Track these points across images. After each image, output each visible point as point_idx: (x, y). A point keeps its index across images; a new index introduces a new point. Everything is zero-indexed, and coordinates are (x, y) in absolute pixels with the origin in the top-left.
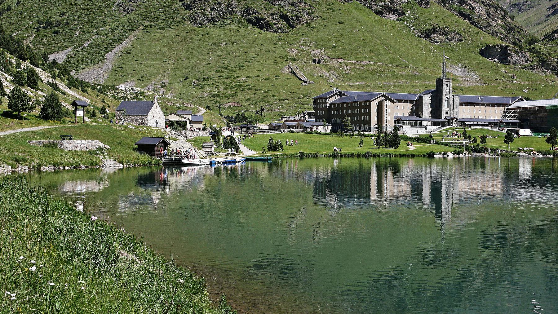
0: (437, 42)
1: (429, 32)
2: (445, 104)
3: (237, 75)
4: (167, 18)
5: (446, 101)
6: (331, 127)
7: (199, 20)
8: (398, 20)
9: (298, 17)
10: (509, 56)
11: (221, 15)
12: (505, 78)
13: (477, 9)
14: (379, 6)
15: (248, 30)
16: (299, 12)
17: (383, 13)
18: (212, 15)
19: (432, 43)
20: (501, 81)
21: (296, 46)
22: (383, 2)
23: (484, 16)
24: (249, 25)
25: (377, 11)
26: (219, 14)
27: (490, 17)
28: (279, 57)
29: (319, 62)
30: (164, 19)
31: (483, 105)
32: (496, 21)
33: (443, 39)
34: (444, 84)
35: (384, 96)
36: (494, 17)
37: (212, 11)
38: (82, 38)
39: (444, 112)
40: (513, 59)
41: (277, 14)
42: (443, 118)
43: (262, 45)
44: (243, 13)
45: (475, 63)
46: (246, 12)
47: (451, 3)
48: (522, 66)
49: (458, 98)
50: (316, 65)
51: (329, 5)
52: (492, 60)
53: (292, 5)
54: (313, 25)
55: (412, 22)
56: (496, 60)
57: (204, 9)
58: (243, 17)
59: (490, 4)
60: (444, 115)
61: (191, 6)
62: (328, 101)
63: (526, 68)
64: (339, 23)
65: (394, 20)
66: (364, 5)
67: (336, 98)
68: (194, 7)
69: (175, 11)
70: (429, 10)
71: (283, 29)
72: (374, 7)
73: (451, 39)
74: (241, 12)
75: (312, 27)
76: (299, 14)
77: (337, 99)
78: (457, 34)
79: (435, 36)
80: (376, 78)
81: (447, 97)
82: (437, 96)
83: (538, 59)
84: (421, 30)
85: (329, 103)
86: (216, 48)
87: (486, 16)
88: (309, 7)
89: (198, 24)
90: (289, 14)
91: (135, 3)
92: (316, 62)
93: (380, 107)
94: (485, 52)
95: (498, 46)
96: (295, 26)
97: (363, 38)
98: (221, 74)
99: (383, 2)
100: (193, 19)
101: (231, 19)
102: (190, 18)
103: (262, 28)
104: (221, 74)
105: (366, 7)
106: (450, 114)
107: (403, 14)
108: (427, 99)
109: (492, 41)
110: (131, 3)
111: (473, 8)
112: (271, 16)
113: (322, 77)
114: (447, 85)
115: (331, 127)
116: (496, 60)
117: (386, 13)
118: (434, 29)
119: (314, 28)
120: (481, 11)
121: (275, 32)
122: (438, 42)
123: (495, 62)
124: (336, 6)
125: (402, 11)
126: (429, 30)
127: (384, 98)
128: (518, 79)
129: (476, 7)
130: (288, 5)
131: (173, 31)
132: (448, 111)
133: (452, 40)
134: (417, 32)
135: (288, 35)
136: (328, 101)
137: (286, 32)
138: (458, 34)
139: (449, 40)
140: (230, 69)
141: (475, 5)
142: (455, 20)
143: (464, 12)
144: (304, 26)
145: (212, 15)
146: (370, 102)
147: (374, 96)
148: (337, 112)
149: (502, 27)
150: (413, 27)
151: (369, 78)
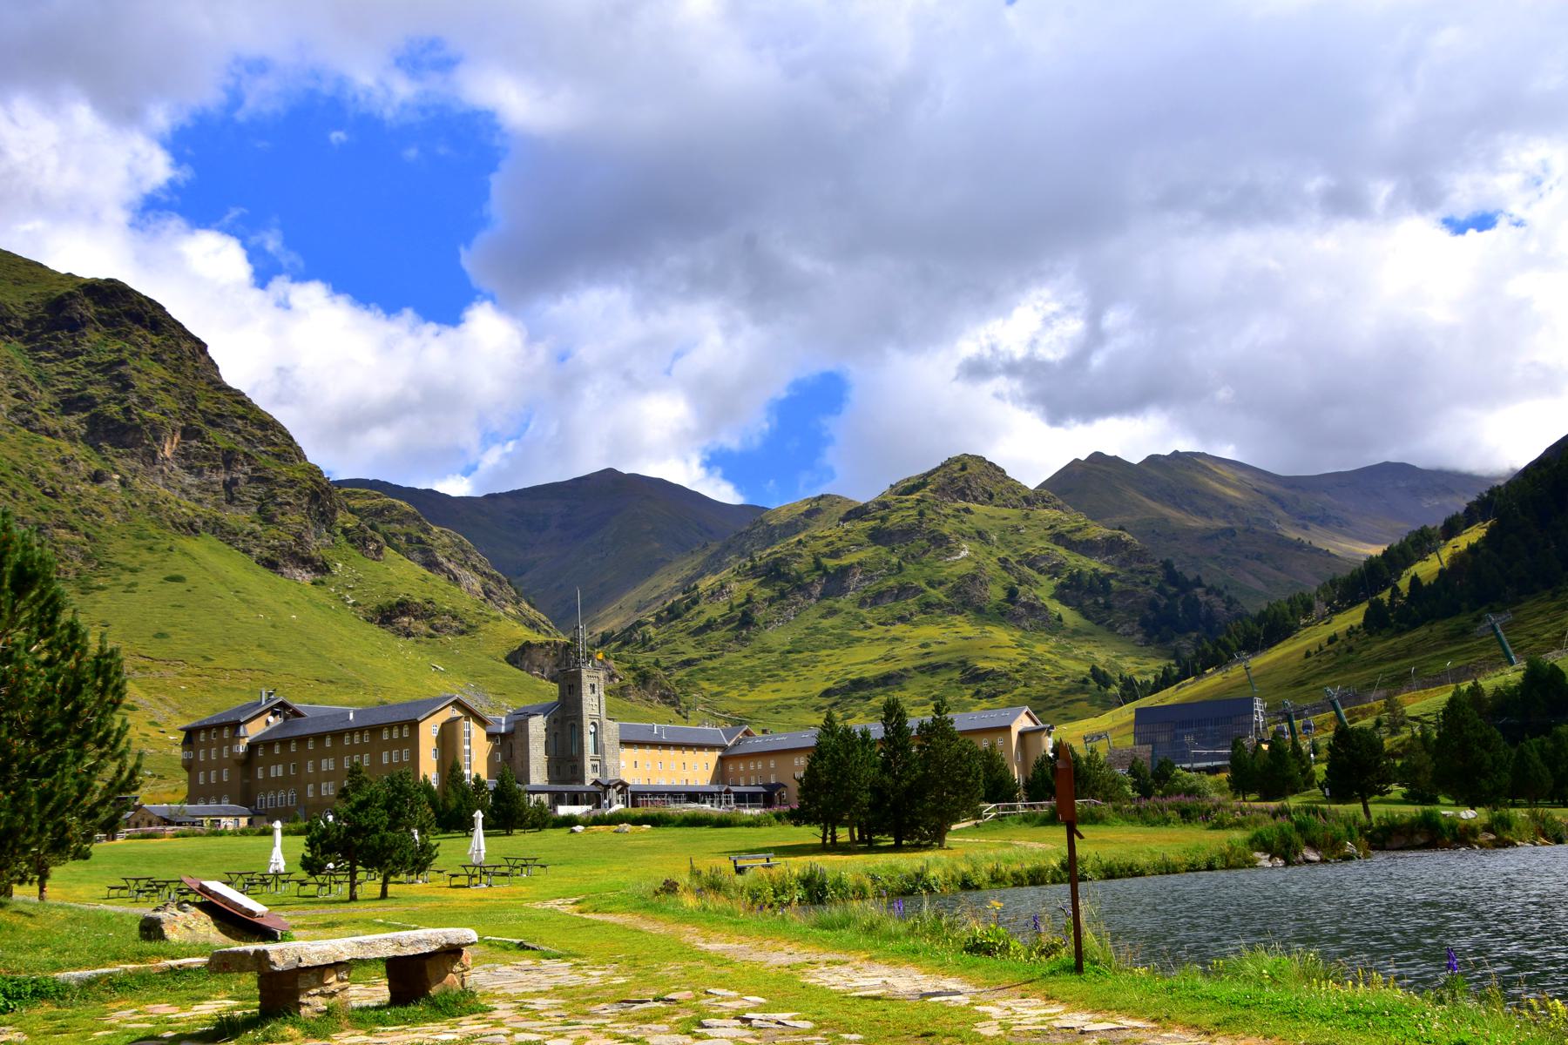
0: (408, 635)
2: (589, 740)
14: (268, 548)
27: (490, 598)
32: (502, 607)
35: (458, 704)
39: (588, 764)
42: (588, 783)
51: (139, 537)
60: (590, 776)
66: (230, 544)
67: (268, 723)
77: (271, 726)
78: (455, 618)
83: (634, 674)
84: (373, 606)
85: (247, 740)
87: (483, 595)
106: (604, 771)
107: (323, 568)
108: (537, 727)
114: (593, 686)
118: (400, 604)
125: (323, 562)
127: (458, 713)
132: (598, 763)
139: (437, 630)
146: (414, 725)
147: (431, 706)
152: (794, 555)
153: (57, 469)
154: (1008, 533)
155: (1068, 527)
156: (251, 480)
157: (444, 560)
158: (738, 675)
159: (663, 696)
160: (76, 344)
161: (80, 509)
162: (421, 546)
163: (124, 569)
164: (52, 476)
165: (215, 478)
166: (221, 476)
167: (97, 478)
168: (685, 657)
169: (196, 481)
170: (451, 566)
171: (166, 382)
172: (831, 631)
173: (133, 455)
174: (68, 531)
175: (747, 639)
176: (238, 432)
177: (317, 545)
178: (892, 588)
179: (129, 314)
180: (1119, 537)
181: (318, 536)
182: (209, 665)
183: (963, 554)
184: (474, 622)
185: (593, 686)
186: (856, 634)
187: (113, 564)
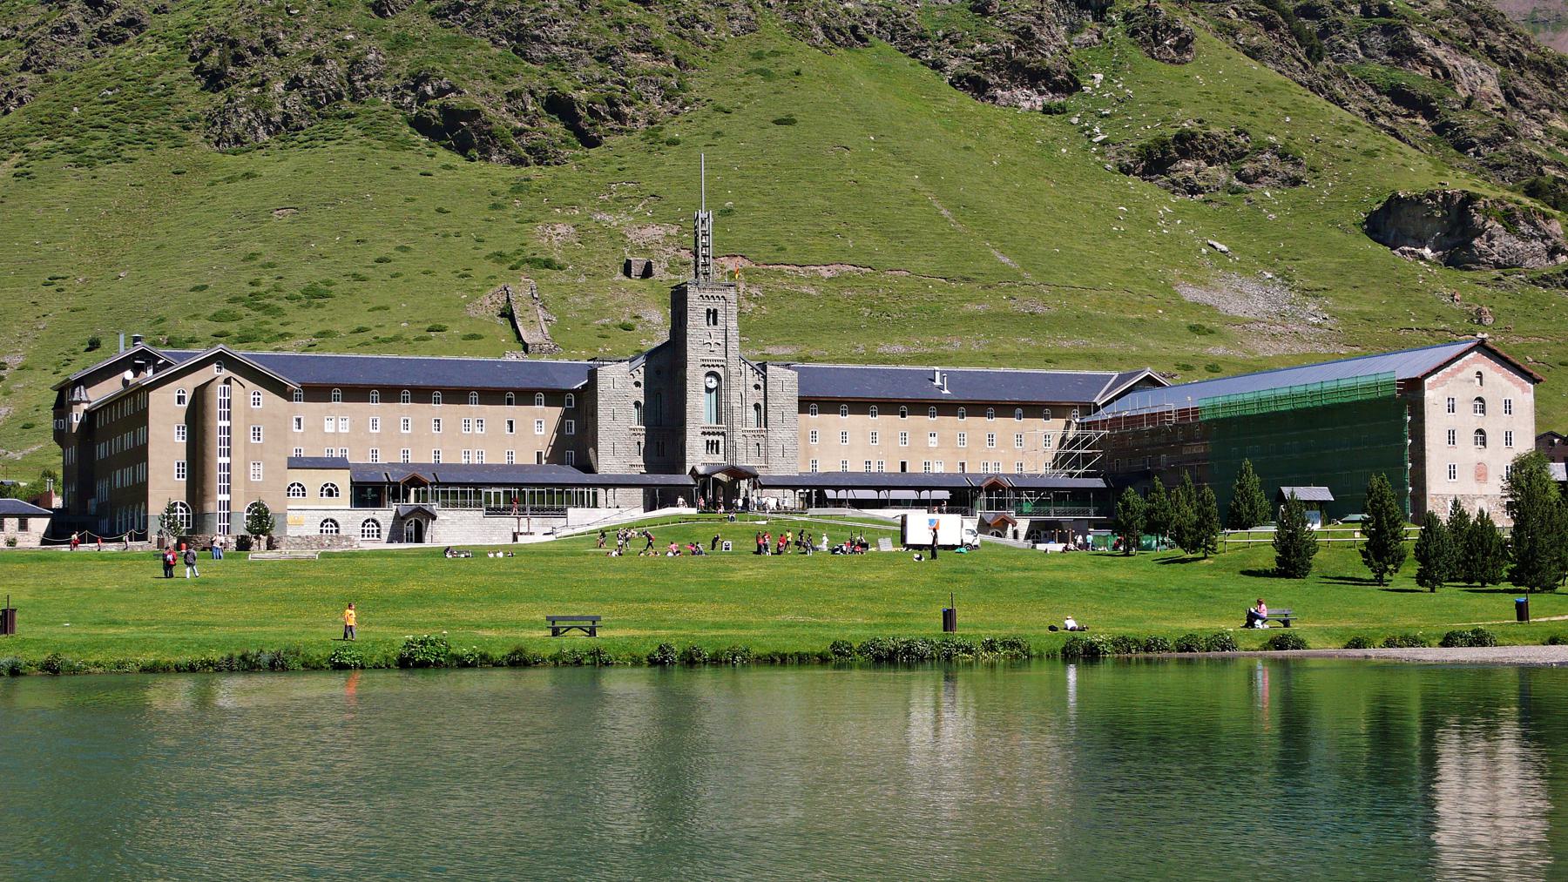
0: (1193, 190)
1: (1164, 153)
3: (283, 330)
4: (120, 120)
5: (709, 390)
6: (47, 520)
7: (237, 126)
8: (1047, 110)
9: (617, 105)
10: (1479, 234)
11: (320, 106)
12: (1445, 321)
13: (1463, 75)
14: (973, 57)
15: (400, 157)
16: (624, 84)
17: (986, 85)
18: (285, 107)
19: (1174, 192)
20: (1425, 333)
21: (577, 212)
22: (988, 41)
23: (1492, 102)
24: (418, 137)
25: (960, 78)
26: (314, 102)
27: (1516, 105)
28: (487, 257)
29: (647, 272)
30: (107, 127)
31: (946, 408)
32: (1542, 121)
33: (1223, 177)
34: (694, 310)
36: (1535, 104)
37: (292, 89)
40: (1493, 245)
41: (532, 93)
43: (440, 211)
44: (403, 96)
45: (1333, 266)
46: (414, 89)
47: (1361, 56)
48: (1532, 276)
49: (791, 376)
50: (636, 282)
51: (758, 56)
52: (1413, 252)
53: (600, 60)
54: (673, 131)
55: (1102, 117)
56: (1427, 252)
57: (262, 84)
58: (401, 107)
59: (1523, 57)
61: (223, 75)
62: (76, 398)
63: (1545, 280)
64: (778, 122)
65: (1032, 109)
66: (914, 56)
68: (234, 80)
69: (158, 96)
70: (1187, 69)
71: (546, 152)
72: (952, 61)
73: (1256, 176)
74: (396, 89)
75: (666, 139)
76: (623, 92)
78: (1283, 156)
79: (1188, 165)
80: (856, 328)
81: (716, 369)
85: (86, 406)
86: (254, 227)
87: (1501, 101)
88: (673, 66)
89: (229, 141)
90: (582, 96)
91: (39, 72)
92: (636, 269)
94: (1385, 223)
95: (1432, 196)
96: (600, 137)
97: (857, 177)
99: (988, 41)
100: (215, 124)
101: (353, 116)
102: (207, 120)
103: (462, 148)
105: (922, 63)
107: (1071, 86)
111: (1446, 74)
112: (509, 101)
114: (712, 315)
115: (47, 520)
116: (1427, 252)
117: (999, 85)
118: (1181, 138)
119: (673, 142)
120: (1479, 82)
121: (513, 162)
122: (1200, 191)
123: (1421, 263)
124: (786, 59)
126: (1164, 143)
128: (1501, 323)
129: (1461, 70)
130: (588, 59)
131: (125, 168)
132: (721, 439)
133: (1260, 180)
134: (1114, 154)
135: (560, 174)
136: (76, 398)
137: (557, 164)
138: (1286, 155)
140: (267, 306)
141: (1457, 60)
142: (1286, 104)
143: (1409, 87)
144: (636, 135)
145: (285, 107)
150: (1104, 134)
151: (823, 328)
157: (1426, 43)
161: (678, 20)
162: (1383, 20)
170: (1439, 53)
174: (650, 55)
185: (712, 315)
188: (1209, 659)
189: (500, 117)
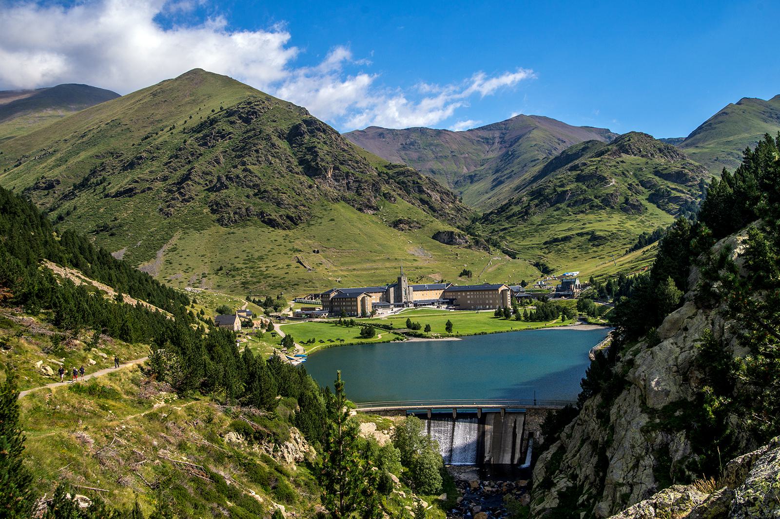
2: (403, 293)
7: (226, 222)
38: (135, 239)
39: (403, 298)
51: (322, 206)
60: (404, 300)
78: (417, 223)
82: (398, 286)
83: (474, 241)
87: (440, 201)
93: (363, 300)
98: (248, 265)
103: (273, 227)
104: (248, 265)
106: (407, 299)
107: (377, 209)
109: (442, 227)
110: (170, 208)
113: (321, 264)
148: (336, 304)
149: (453, 209)
152: (547, 186)
153: (300, 186)
154: (91, 449)
155: (662, 167)
156: (354, 181)
158: (520, 234)
159: (484, 248)
160: (302, 141)
163: (319, 217)
164: (298, 189)
165: (343, 182)
166: (345, 182)
167: (310, 187)
168: (504, 227)
169: (338, 184)
170: (429, 191)
171: (328, 152)
172: (556, 217)
173: (320, 178)
175: (526, 220)
176: (350, 165)
177: (374, 202)
178: (581, 199)
179: (316, 128)
180: (682, 172)
181: (375, 197)
182: (341, 248)
183: (611, 184)
184: (424, 224)
186: (564, 218)
187: (316, 216)
188: (536, 141)
189: (280, 221)
